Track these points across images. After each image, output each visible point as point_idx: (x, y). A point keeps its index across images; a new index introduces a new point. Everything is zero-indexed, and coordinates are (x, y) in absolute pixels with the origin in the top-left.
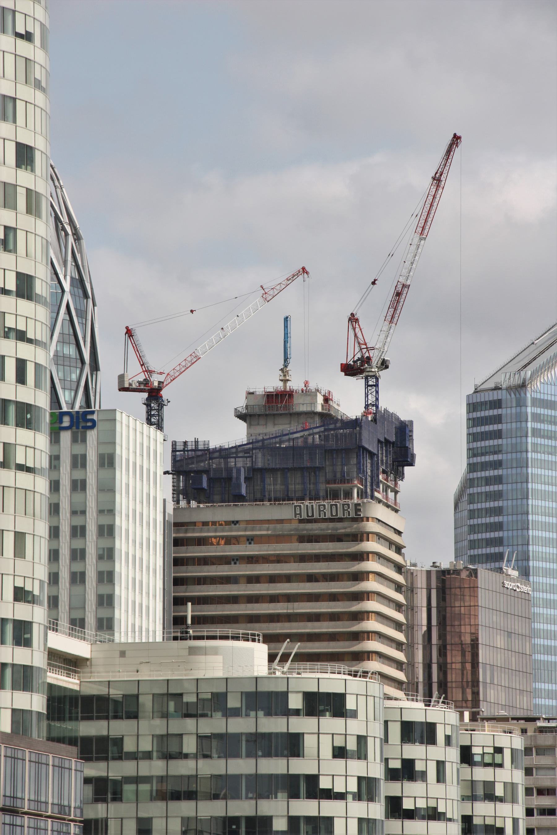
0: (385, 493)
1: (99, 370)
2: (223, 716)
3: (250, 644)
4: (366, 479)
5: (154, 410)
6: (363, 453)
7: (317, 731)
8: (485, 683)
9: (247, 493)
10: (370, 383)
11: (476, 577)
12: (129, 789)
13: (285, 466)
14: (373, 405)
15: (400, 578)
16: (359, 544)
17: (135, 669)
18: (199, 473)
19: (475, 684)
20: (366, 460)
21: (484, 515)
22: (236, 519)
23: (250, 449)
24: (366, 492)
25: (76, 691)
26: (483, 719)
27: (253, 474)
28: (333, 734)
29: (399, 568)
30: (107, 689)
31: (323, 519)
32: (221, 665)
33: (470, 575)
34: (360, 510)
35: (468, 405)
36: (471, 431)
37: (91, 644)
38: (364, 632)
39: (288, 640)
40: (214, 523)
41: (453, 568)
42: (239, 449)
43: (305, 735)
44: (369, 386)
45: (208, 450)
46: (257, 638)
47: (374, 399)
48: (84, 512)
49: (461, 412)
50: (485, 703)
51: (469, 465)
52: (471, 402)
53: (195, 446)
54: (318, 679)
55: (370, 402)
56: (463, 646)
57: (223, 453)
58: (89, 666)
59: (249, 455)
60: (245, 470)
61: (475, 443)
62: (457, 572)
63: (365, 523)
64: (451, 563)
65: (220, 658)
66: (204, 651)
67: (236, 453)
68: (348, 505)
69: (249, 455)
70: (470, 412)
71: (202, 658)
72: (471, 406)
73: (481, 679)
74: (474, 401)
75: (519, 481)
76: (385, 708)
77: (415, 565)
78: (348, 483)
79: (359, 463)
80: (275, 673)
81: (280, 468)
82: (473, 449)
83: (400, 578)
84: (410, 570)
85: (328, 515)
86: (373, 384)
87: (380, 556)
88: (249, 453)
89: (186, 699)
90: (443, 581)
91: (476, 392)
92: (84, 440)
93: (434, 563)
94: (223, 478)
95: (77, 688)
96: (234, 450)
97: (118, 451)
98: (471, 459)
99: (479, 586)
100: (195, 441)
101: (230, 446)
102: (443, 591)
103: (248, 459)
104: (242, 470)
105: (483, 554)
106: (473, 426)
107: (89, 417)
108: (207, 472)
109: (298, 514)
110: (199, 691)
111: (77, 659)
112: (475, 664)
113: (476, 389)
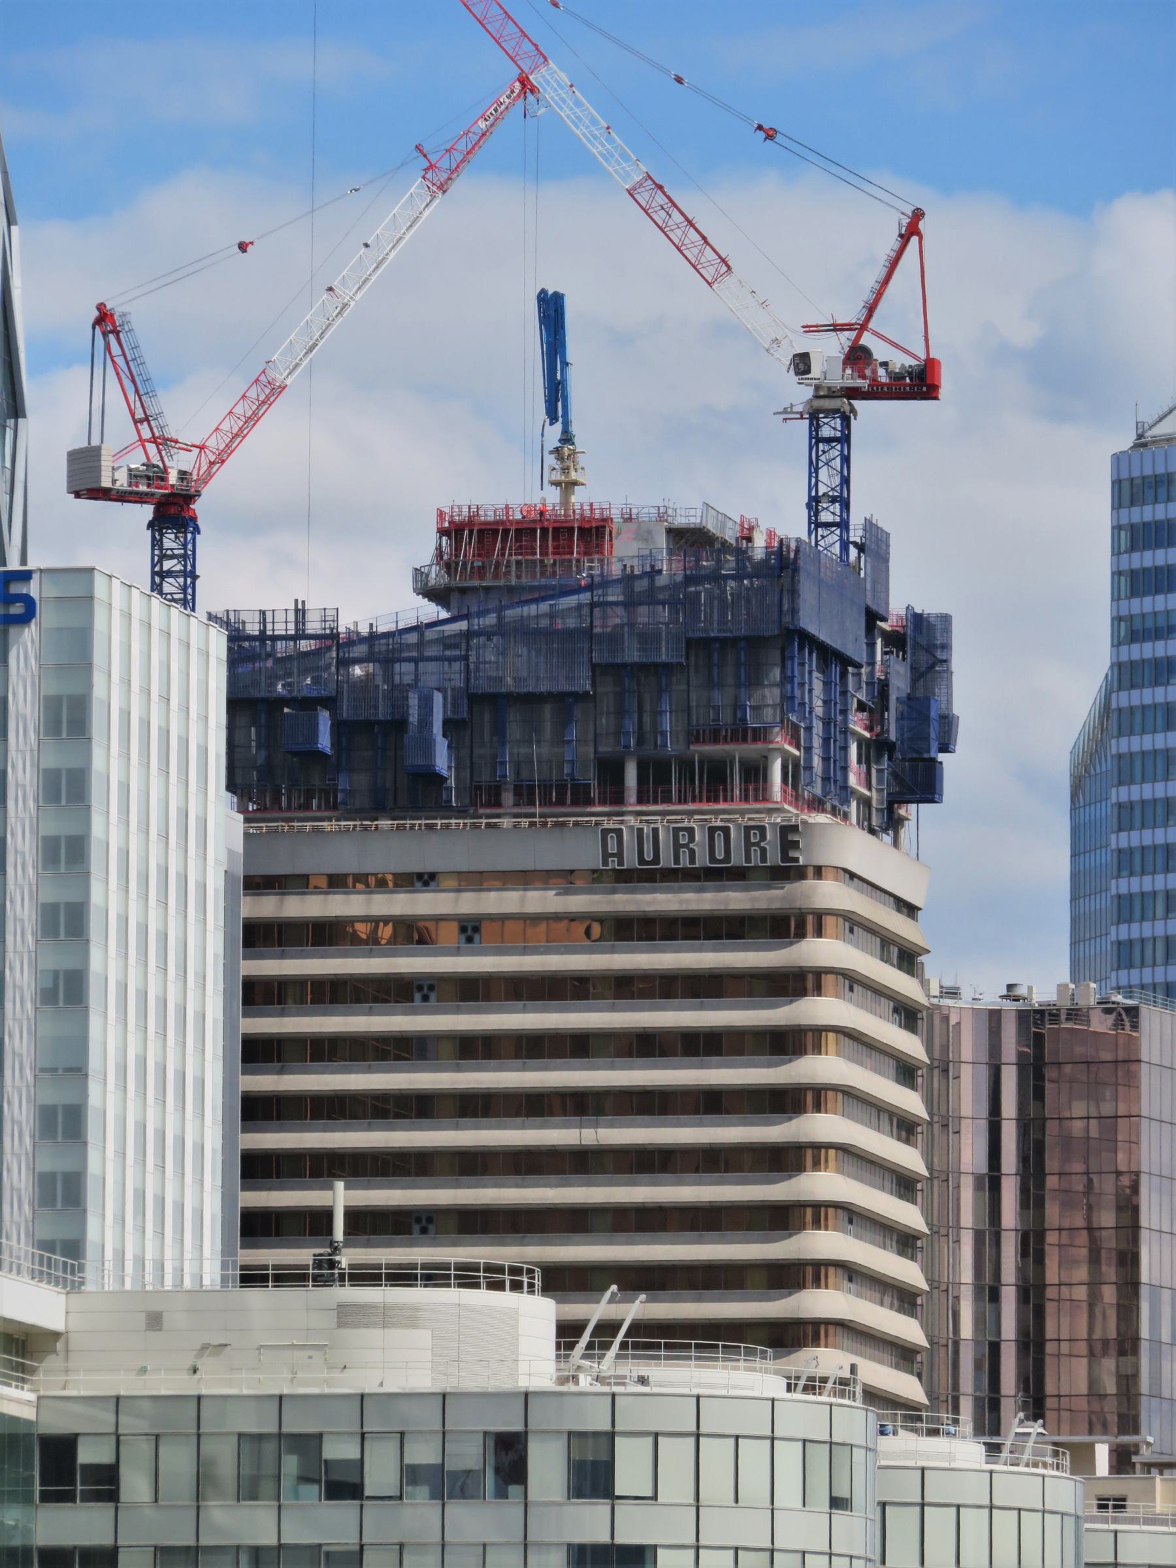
0: (864, 767)
1: (24, 416)
2: (433, 1496)
3: (506, 1299)
4: (809, 729)
5: (172, 557)
6: (801, 649)
7: (692, 1541)
8: (1156, 1342)
9: (450, 768)
10: (826, 432)
11: (1135, 1026)
13: (568, 688)
14: (833, 500)
15: (911, 1045)
16: (791, 944)
17: (189, 1363)
18: (308, 704)
19: (1128, 1346)
20: (810, 672)
21: (1159, 819)
22: (430, 868)
23: (461, 634)
24: (809, 768)
25: (28, 1423)
26: (1148, 1466)
27: (471, 711)
28: (737, 1549)
29: (908, 1014)
30: (112, 1417)
32: (428, 1356)
33: (1118, 1023)
34: (795, 845)
35: (1117, 484)
36: (1124, 563)
37: (68, 1293)
38: (802, 1205)
39: (614, 1288)
40: (361, 878)
41: (1068, 1004)
42: (430, 634)
43: (660, 1551)
45: (334, 636)
46: (525, 1280)
47: (837, 480)
49: (1092, 516)
50: (1154, 1401)
51: (1118, 667)
52: (1124, 475)
53: (297, 622)
54: (698, 1397)
55: (822, 489)
56: (1097, 1233)
57: (381, 646)
58: (62, 1354)
59: (457, 653)
60: (445, 698)
61: (1136, 602)
62: (1074, 1014)
63: (810, 883)
64: (1062, 988)
65: (423, 1337)
66: (385, 1317)
67: (421, 644)
68: (762, 829)
69: (457, 653)
70: (1120, 506)
71: (374, 1336)
72: (1126, 487)
73: (1145, 1333)
74: (1136, 473)
76: (879, 1468)
77: (953, 993)
78: (755, 739)
79: (787, 679)
80: (575, 1379)
81: (550, 694)
82: (1133, 574)
83: (911, 1045)
84: (939, 1007)
85: (702, 860)
86: (832, 434)
87: (852, 981)
88: (456, 646)
90: (1039, 1039)
91: (1141, 444)
93: (1010, 987)
94: (379, 722)
95: (28, 1414)
96: (413, 638)
97: (98, 691)
98: (1124, 649)
99: (1144, 1057)
100: (297, 610)
101: (401, 626)
102: (1034, 1073)
103: (456, 666)
104: (438, 698)
105: (1155, 847)
106: (1133, 548)
107: (16, 588)
108: (330, 703)
109: (613, 855)
111: (27, 1335)
112: (1130, 1286)
113: (1140, 436)
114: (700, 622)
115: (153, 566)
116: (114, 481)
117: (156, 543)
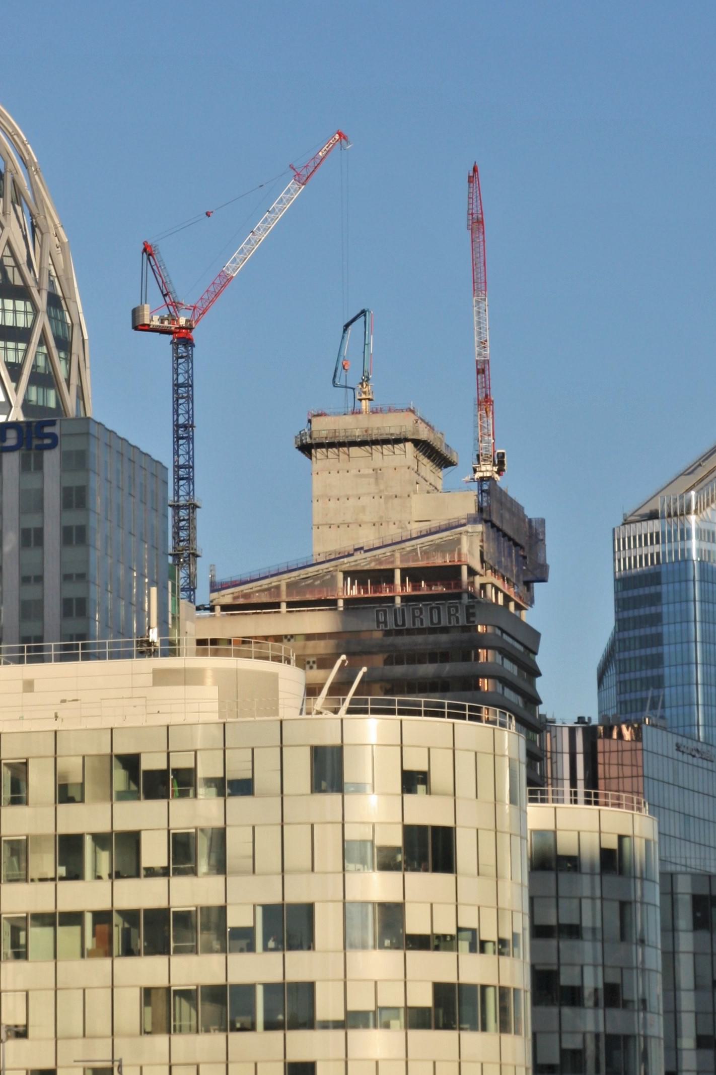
5: (184, 520)
12: (38, 937)
21: (638, 688)
31: (418, 629)
44: (483, 491)
48: (39, 579)
75: (641, 779)
85: (427, 624)
89: (146, 764)
92: (40, 467)
107: (47, 430)
110: (170, 749)
114: (429, 586)
115: (174, 462)
116: (151, 320)
117: (175, 350)
